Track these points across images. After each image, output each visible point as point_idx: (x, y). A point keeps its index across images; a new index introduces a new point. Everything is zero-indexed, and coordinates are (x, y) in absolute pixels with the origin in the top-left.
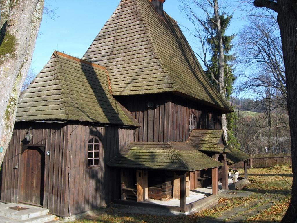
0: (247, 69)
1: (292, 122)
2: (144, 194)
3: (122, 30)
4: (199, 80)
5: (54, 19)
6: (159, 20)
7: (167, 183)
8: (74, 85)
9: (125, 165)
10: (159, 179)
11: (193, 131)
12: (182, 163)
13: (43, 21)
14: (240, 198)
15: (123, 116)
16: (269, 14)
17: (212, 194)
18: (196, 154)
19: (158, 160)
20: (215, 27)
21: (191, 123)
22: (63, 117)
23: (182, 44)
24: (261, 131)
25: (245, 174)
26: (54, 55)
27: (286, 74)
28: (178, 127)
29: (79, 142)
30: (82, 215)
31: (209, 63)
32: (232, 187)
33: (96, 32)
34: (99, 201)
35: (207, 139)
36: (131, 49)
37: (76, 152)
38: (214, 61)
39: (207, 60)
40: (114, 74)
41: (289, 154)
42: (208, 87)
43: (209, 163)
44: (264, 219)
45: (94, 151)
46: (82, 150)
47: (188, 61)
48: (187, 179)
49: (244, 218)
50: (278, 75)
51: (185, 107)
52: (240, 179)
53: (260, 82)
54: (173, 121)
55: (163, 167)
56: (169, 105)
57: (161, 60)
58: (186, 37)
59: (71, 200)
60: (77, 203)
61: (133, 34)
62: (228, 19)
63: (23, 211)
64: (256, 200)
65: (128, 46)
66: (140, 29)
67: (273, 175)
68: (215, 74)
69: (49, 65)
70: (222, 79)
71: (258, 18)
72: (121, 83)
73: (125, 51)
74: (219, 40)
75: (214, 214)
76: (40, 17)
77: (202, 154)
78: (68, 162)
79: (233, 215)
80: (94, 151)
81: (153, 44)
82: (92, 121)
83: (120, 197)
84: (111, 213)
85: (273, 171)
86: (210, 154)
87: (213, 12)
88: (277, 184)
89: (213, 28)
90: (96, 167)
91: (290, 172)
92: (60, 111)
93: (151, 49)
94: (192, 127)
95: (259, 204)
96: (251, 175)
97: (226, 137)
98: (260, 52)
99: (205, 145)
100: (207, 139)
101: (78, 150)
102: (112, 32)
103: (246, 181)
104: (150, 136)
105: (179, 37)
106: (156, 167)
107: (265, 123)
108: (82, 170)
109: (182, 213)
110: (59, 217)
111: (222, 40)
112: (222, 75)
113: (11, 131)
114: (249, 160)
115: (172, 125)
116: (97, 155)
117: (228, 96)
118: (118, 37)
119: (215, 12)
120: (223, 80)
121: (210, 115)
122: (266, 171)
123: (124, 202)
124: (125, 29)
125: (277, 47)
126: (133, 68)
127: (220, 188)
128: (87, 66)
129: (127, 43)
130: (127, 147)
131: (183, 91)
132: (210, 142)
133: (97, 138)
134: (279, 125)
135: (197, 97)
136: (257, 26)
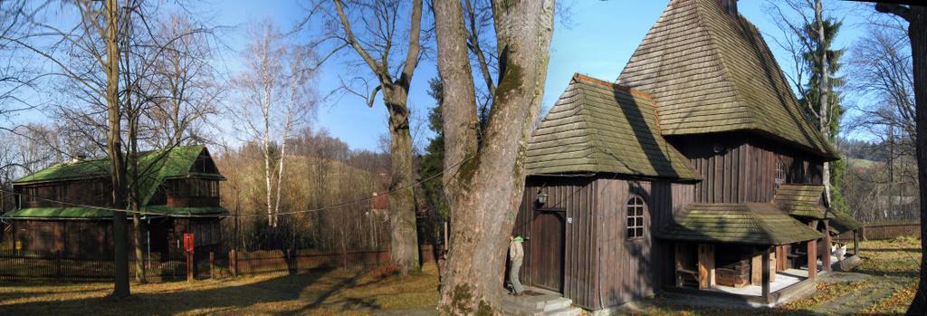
0: (861, 98)
1: (922, 175)
2: (709, 278)
3: (674, 40)
4: (790, 113)
5: (571, 29)
6: (731, 25)
7: (743, 262)
8: (605, 121)
9: (680, 237)
10: (732, 256)
11: (781, 187)
12: (764, 234)
13: (556, 33)
14: (848, 283)
15: (678, 165)
16: (896, 23)
17: (807, 278)
18: (785, 220)
19: (730, 230)
20: (815, 37)
21: (777, 175)
22: (590, 168)
23: (765, 60)
24: (879, 188)
25: (855, 249)
26: (573, 79)
27: (917, 108)
28: (759, 180)
29: (613, 204)
30: (619, 308)
31: (805, 88)
32: (836, 267)
33: (636, 43)
34: (643, 289)
35: (800, 198)
36: (688, 67)
37: (610, 217)
38: (813, 84)
39: (802, 83)
40: (664, 104)
41: (918, 221)
42: (804, 123)
43: (804, 233)
44: (882, 311)
45: (635, 217)
46: (619, 215)
47: (774, 85)
48: (772, 256)
49: (854, 311)
50: (905, 109)
52: (848, 255)
53: (880, 118)
54: (751, 172)
55: (737, 239)
56: (746, 149)
57: (733, 83)
58: (771, 50)
59: (603, 286)
60: (613, 291)
61: (691, 46)
62: (836, 27)
63: (539, 297)
64: (871, 286)
65: (684, 63)
66: (702, 38)
67: (895, 250)
68: (813, 105)
69: (567, 94)
70: (824, 112)
71: (881, 28)
72: (673, 116)
73: (679, 70)
74: (821, 55)
75: (811, 305)
76: (550, 28)
77: (793, 220)
78: (598, 233)
79: (838, 307)
80: (635, 217)
81: (722, 60)
82: (632, 173)
83: (674, 283)
84: (662, 305)
85: (895, 245)
86: (805, 220)
87: (813, 16)
88: (900, 263)
89: (812, 39)
90: (639, 240)
91: (919, 245)
92: (586, 160)
93: (719, 67)
94: (779, 181)
95: (875, 290)
96: (864, 250)
97: (828, 196)
98: (880, 75)
99: (798, 208)
100: (800, 198)
101: (612, 214)
102: (659, 44)
103: (856, 259)
104: (718, 193)
105: (761, 49)
106: (727, 239)
107: (885, 176)
108: (619, 243)
109: (765, 305)
110: (587, 310)
111: (825, 56)
112: (825, 106)
113: (521, 191)
114: (861, 229)
115: (751, 178)
116: (640, 222)
117: (833, 136)
118: (669, 51)
119: (816, 16)
120: (825, 114)
121: (806, 164)
122: (884, 245)
123: (680, 290)
124: (679, 39)
125: (906, 70)
126: (692, 94)
127: (820, 268)
128: (623, 94)
129: (682, 59)
130: (685, 211)
131: (766, 129)
132: (805, 203)
133: (640, 198)
134: (905, 180)
135: (787, 138)
136: (878, 38)
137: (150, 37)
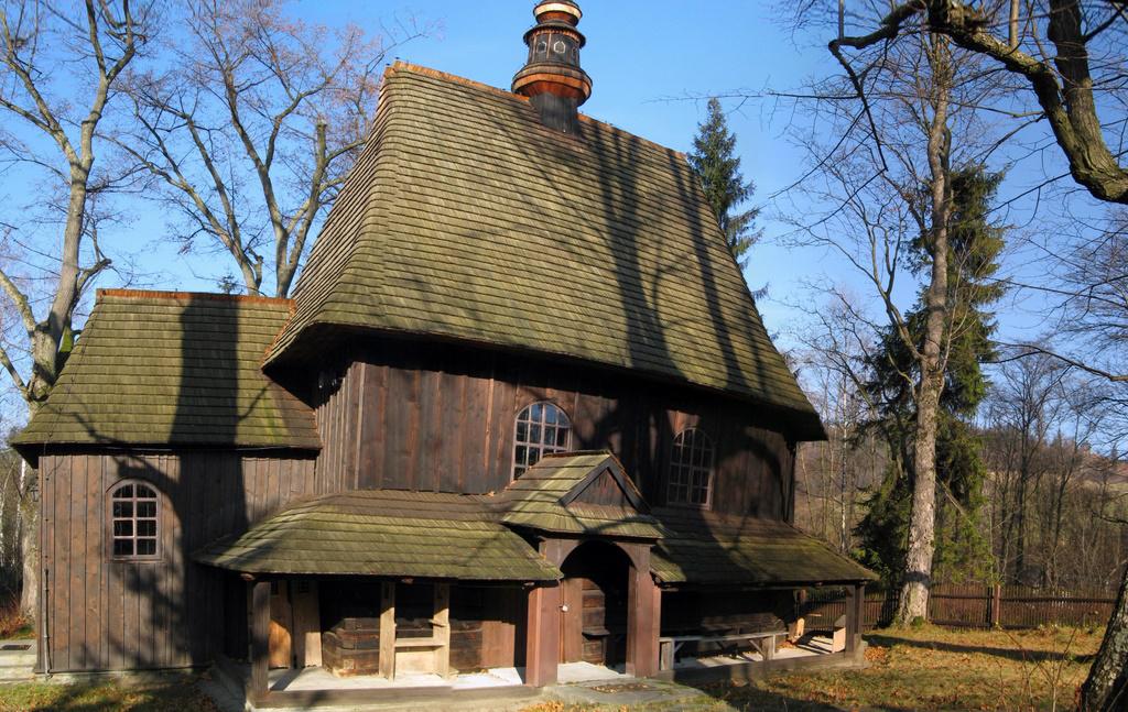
51: (470, 376)
90: (151, 561)
95: (948, 683)
137: (856, 130)
